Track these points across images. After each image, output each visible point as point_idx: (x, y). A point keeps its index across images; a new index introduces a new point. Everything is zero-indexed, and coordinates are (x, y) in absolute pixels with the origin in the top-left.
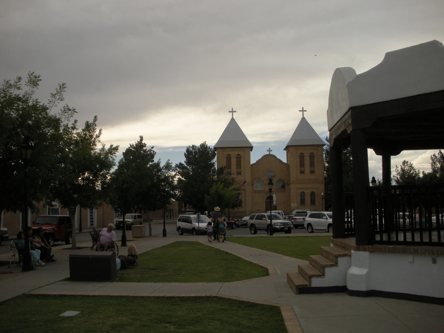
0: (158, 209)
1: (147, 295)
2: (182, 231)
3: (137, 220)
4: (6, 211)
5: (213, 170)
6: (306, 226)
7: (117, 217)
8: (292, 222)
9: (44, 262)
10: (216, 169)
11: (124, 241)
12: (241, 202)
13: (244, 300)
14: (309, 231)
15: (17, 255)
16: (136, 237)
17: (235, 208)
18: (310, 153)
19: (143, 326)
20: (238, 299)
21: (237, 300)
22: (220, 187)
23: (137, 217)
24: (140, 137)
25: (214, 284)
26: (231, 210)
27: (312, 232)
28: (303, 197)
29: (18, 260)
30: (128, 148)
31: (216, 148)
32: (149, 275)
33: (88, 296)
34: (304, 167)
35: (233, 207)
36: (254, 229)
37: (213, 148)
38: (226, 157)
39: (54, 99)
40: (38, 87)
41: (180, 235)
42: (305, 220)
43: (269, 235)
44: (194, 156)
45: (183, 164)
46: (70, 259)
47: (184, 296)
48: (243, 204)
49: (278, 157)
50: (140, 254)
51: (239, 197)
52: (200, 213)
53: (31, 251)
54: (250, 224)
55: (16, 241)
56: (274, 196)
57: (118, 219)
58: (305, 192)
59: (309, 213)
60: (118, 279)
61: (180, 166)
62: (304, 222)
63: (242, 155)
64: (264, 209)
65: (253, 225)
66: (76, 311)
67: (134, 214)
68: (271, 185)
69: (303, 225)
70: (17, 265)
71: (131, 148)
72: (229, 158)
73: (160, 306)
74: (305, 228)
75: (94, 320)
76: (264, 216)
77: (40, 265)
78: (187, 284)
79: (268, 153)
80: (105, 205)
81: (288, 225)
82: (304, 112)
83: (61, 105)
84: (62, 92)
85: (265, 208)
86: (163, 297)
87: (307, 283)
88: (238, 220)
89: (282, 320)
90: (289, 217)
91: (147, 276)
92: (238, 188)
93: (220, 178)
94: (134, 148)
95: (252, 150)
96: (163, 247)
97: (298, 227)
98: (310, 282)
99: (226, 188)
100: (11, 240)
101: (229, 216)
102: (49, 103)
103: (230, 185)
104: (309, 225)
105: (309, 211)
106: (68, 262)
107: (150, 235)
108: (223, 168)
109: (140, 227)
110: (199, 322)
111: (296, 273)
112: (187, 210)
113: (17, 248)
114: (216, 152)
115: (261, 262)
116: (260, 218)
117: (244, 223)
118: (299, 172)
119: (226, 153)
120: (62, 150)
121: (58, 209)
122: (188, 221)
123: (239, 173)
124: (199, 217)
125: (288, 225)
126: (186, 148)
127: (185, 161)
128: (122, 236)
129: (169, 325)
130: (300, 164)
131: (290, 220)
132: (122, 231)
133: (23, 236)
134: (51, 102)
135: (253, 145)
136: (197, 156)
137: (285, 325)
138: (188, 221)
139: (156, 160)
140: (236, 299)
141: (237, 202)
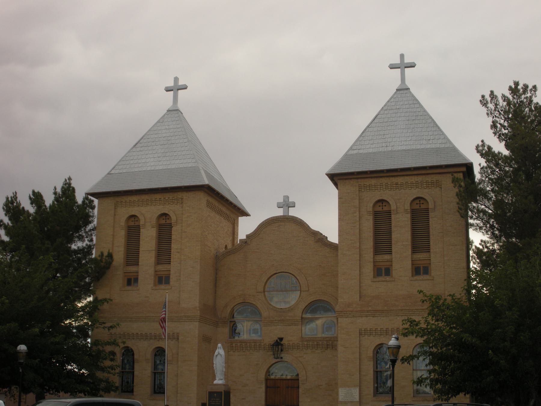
34: (390, 253)
79: (280, 212)
118: (369, 269)
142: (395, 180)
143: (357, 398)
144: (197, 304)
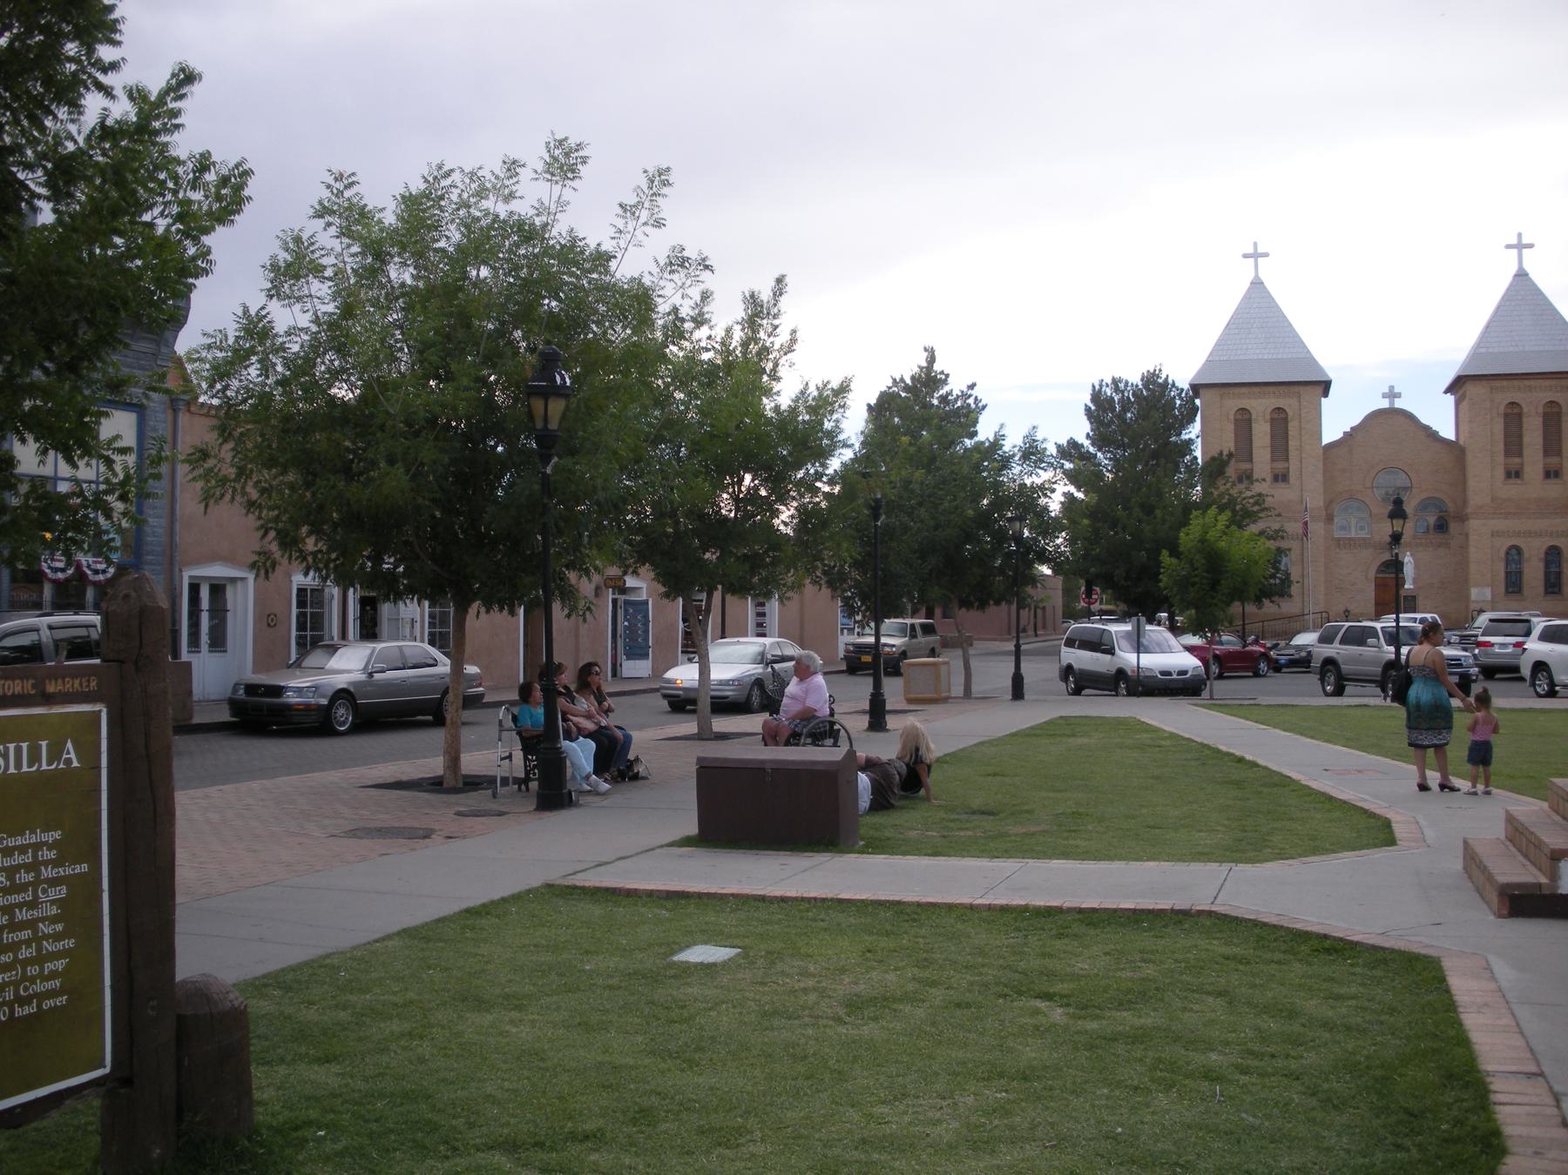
0: (998, 603)
1: (966, 900)
2: (1080, 682)
3: (922, 639)
4: (483, 609)
5: (1187, 466)
6: (1526, 672)
7: (851, 631)
8: (1475, 656)
9: (606, 781)
10: (1200, 461)
11: (877, 715)
12: (1287, 581)
13: (1309, 929)
14: (1539, 689)
15: (518, 755)
16: (917, 701)
17: (1266, 602)
18: (1544, 402)
19: (959, 1005)
20: (1286, 925)
21: (1282, 927)
22: (1216, 525)
23: (918, 629)
24: (926, 350)
25: (1197, 867)
26: (1251, 608)
27: (1552, 693)
28: (1514, 566)
29: (522, 775)
30: (884, 388)
31: (1196, 388)
32: (969, 833)
33: (762, 899)
35: (1258, 600)
36: (1335, 677)
37: (1186, 386)
38: (1236, 420)
39: (630, 223)
40: (575, 183)
41: (1070, 694)
42: (1525, 649)
43: (1389, 699)
44: (1121, 417)
45: (1082, 446)
46: (698, 771)
47: (1095, 905)
48: (1294, 589)
49: (1424, 420)
50: (938, 760)
51: (1280, 562)
52: (1143, 619)
53: (565, 744)
54: (1322, 659)
55: (516, 710)
56: (1406, 560)
57: (852, 637)
58: (1523, 546)
59: (1539, 624)
60: (862, 843)
61: (1071, 450)
62: (1517, 656)
63: (1290, 413)
64: (1371, 609)
65: (1329, 662)
66: (726, 946)
67: (909, 621)
68: (1401, 521)
69: (1516, 669)
70: (520, 789)
71: (896, 389)
72: (1244, 422)
73: (1013, 938)
74: (1522, 679)
75: (788, 980)
76: (1372, 633)
77: (595, 792)
78: (1103, 865)
79: (1385, 404)
80: (809, 589)
81: (1460, 666)
82: (1525, 251)
83: (657, 245)
84: (658, 198)
85: (1373, 602)
86: (1025, 908)
87: (1544, 880)
88: (1275, 646)
89: (1451, 1006)
90: (1463, 637)
91: (962, 833)
92: (1277, 531)
93: (1212, 493)
94: (907, 388)
95: (1326, 394)
96: (1013, 735)
97: (1498, 676)
98: (1554, 876)
99: (1234, 528)
100: (498, 704)
101: (1244, 629)
102: (617, 235)
103: (1247, 520)
104: (1540, 667)
105: (1539, 616)
106: (694, 782)
107: (968, 693)
108: (1225, 458)
109: (934, 664)
110: (1151, 998)
111: (1498, 839)
112: (1095, 607)
113: (519, 733)
114: (1198, 402)
115: (1367, 797)
116: (1359, 637)
117: (1297, 656)
119: (1234, 403)
120: (663, 400)
121: (646, 603)
122: (1100, 644)
123: (1281, 477)
124: (1138, 631)
125: (1460, 666)
126: (1091, 388)
127: (1088, 434)
128: (872, 695)
129: (1048, 1003)
130: (1505, 445)
131: (1465, 650)
132: (870, 680)
133: (538, 693)
134: (621, 232)
135: (1332, 375)
136: (1129, 415)
137: (1461, 1025)
138: (1100, 644)
139: (985, 431)
140: (1280, 923)
141: (1272, 581)
142: (1526, 383)
143: (1489, 598)
144: (1322, 504)
